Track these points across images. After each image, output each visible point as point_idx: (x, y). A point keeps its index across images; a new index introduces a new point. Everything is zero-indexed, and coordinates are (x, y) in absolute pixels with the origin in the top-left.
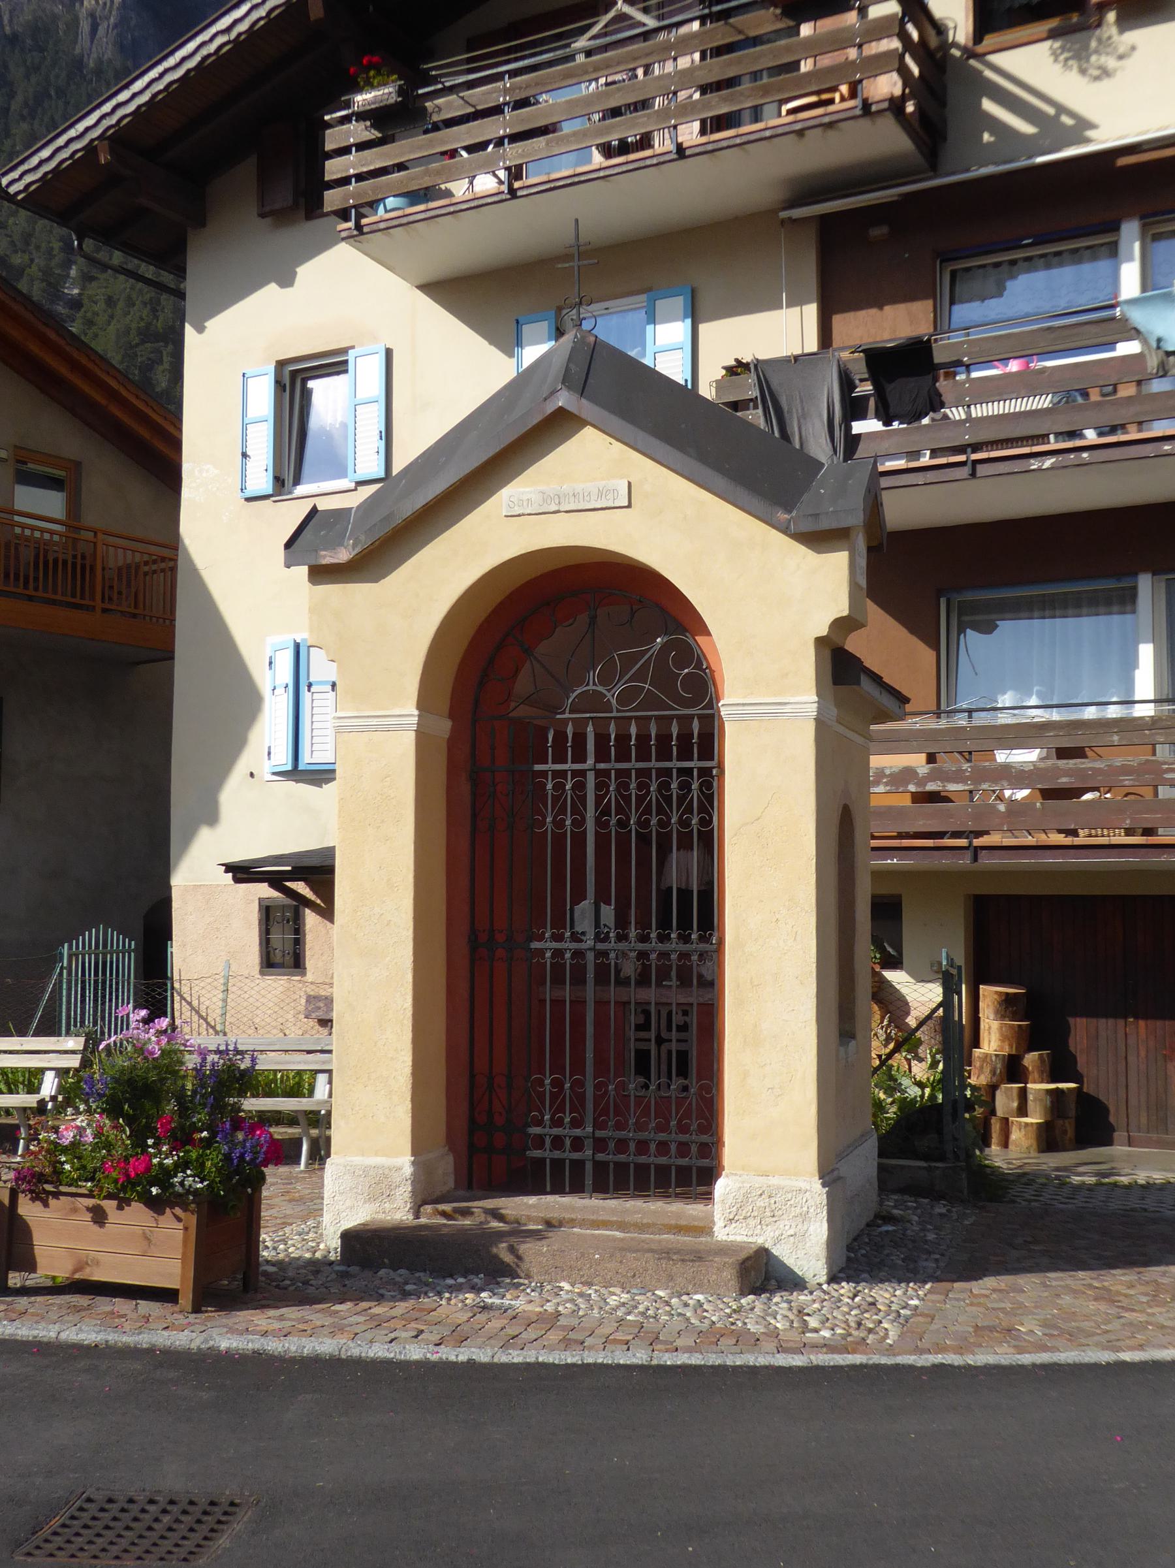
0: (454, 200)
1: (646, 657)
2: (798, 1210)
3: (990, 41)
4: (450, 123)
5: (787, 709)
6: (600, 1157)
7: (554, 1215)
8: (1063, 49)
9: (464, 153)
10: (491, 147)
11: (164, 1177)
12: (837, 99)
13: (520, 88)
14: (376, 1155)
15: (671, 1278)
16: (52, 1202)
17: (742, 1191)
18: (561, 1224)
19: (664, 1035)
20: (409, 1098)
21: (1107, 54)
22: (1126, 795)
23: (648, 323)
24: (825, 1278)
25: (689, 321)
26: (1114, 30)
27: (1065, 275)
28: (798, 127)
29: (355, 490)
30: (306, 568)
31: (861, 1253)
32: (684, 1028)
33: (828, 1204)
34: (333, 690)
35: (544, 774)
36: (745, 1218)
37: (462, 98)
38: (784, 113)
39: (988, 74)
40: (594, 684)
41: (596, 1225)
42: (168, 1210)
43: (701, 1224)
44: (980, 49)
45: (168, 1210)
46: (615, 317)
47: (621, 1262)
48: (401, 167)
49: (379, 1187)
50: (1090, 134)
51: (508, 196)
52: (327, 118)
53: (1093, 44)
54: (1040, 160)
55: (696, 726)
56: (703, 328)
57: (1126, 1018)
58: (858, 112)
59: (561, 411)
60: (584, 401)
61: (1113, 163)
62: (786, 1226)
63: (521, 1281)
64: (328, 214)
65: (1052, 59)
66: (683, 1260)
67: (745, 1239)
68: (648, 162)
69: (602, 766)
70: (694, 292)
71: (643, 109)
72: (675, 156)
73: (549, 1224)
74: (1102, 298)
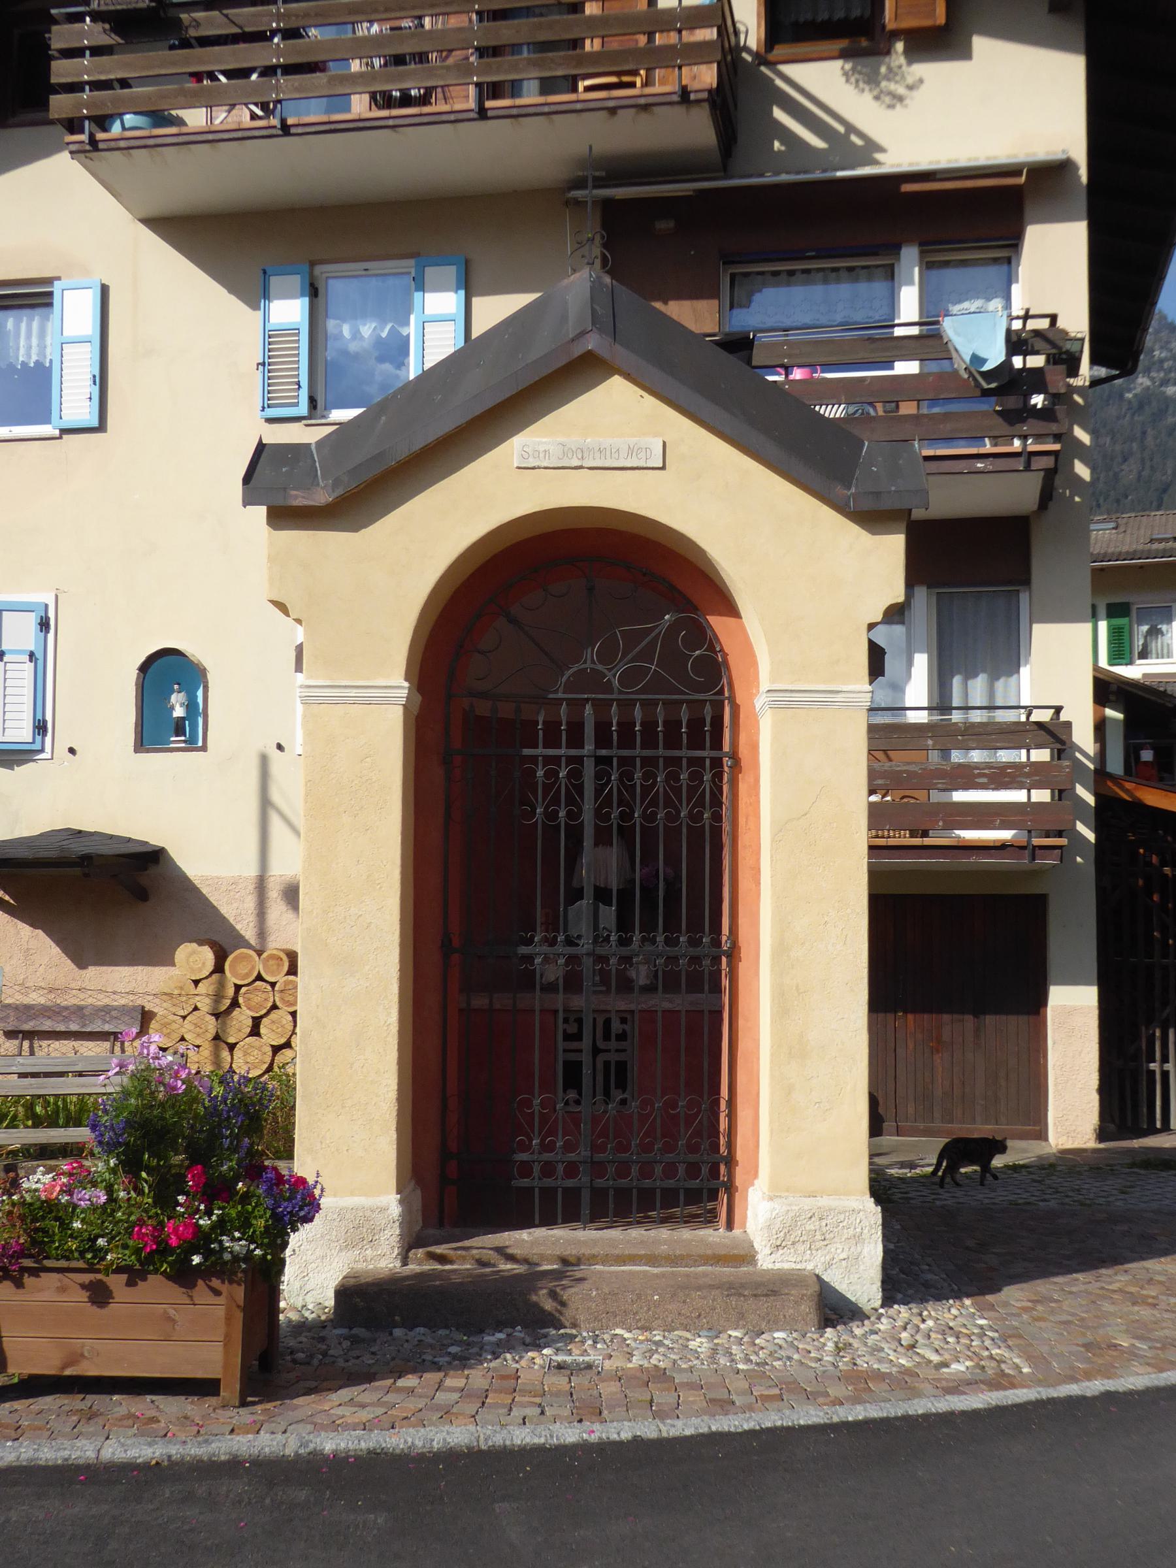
0: (184, 130)
1: (653, 634)
2: (851, 1232)
3: (779, 51)
4: (205, 42)
5: (839, 698)
6: (600, 1183)
7: (570, 1252)
8: (853, 69)
9: (223, 79)
10: (254, 77)
11: (201, 1241)
12: (639, 84)
13: (297, 16)
14: (352, 1194)
15: (742, 1316)
16: (28, 1280)
17: (791, 1214)
18: (579, 1261)
19: (601, 1044)
20: (394, 1127)
21: (897, 82)
22: (902, 798)
23: (417, 290)
24: (880, 1302)
25: (462, 293)
26: (902, 60)
27: (843, 291)
28: (611, 104)
29: (60, 438)
30: (264, 508)
31: (910, 1274)
32: (622, 1037)
33: (883, 1225)
34: (31, 661)
35: (533, 759)
36: (793, 1243)
37: (226, 16)
38: (581, 88)
39: (779, 83)
40: (593, 662)
41: (622, 1260)
42: (200, 1282)
43: (742, 1253)
44: (771, 57)
45: (200, 1282)
46: (374, 281)
47: (684, 1302)
48: (124, 83)
49: (359, 1231)
50: (879, 156)
51: (280, 132)
52: (53, 11)
53: (883, 70)
54: (840, 174)
55: (638, 713)
56: (476, 301)
57: (896, 1012)
58: (675, 98)
59: (589, 353)
60: (618, 347)
61: (898, 188)
62: (839, 1250)
63: (568, 1331)
64: (52, 122)
65: (844, 79)
66: (755, 1296)
67: (793, 1266)
68: (444, 117)
69: (604, 752)
70: (467, 262)
71: (421, 62)
72: (476, 116)
73: (565, 1261)
74: (877, 318)
